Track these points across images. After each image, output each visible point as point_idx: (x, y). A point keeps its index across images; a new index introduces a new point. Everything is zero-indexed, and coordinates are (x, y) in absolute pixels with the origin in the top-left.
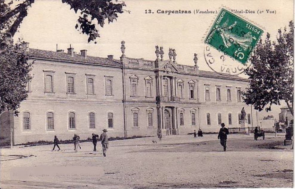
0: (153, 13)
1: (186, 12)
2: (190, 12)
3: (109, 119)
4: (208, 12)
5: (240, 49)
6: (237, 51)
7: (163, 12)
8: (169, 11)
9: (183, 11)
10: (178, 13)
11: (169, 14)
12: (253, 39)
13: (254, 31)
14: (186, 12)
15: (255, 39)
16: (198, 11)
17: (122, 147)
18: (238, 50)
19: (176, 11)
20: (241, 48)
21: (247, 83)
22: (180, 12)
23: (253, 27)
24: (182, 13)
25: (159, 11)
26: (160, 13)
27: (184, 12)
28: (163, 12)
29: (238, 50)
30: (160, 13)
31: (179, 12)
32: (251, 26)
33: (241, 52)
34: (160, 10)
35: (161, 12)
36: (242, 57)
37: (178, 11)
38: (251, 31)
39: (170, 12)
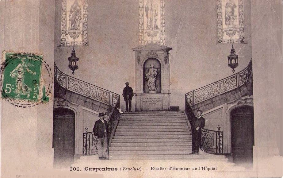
0: (81, 170)
1: (112, 169)
2: (116, 169)
3: (252, 94)
4: (134, 169)
5: (13, 86)
6: (10, 85)
7: (90, 169)
8: (96, 169)
9: (110, 168)
10: (105, 170)
11: (96, 171)
12: (27, 95)
13: (35, 93)
14: (112, 169)
15: (28, 97)
16: (124, 168)
17: (206, 113)
18: (11, 85)
19: (103, 169)
20: (15, 88)
21: (190, 143)
22: (107, 169)
23: (37, 90)
24: (109, 170)
25: (87, 169)
26: (88, 170)
27: (111, 169)
28: (90, 169)
29: (11, 85)
30: (88, 170)
31: (106, 169)
32: (37, 88)
33: (11, 89)
34: (88, 168)
35: (88, 169)
36: (7, 92)
37: (105, 169)
38: (33, 90)
39: (97, 169)
